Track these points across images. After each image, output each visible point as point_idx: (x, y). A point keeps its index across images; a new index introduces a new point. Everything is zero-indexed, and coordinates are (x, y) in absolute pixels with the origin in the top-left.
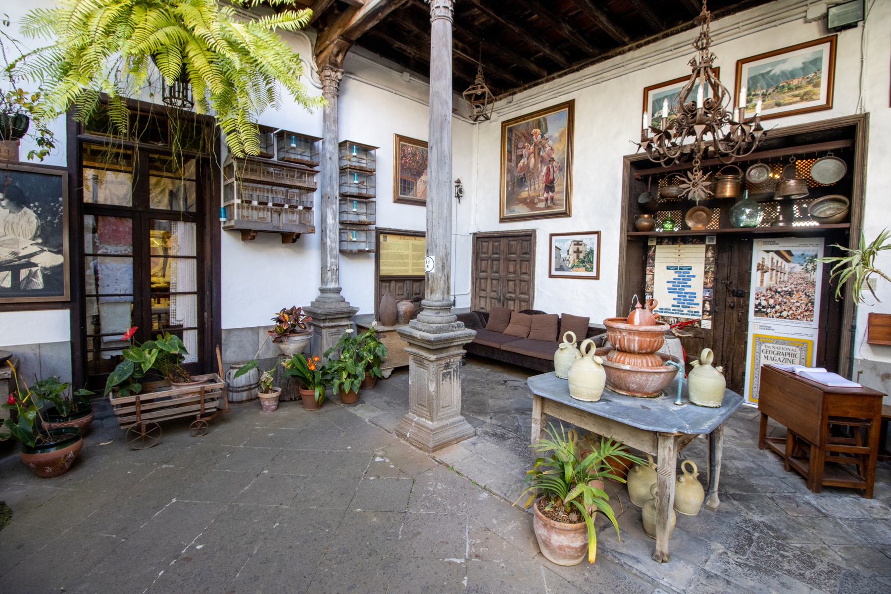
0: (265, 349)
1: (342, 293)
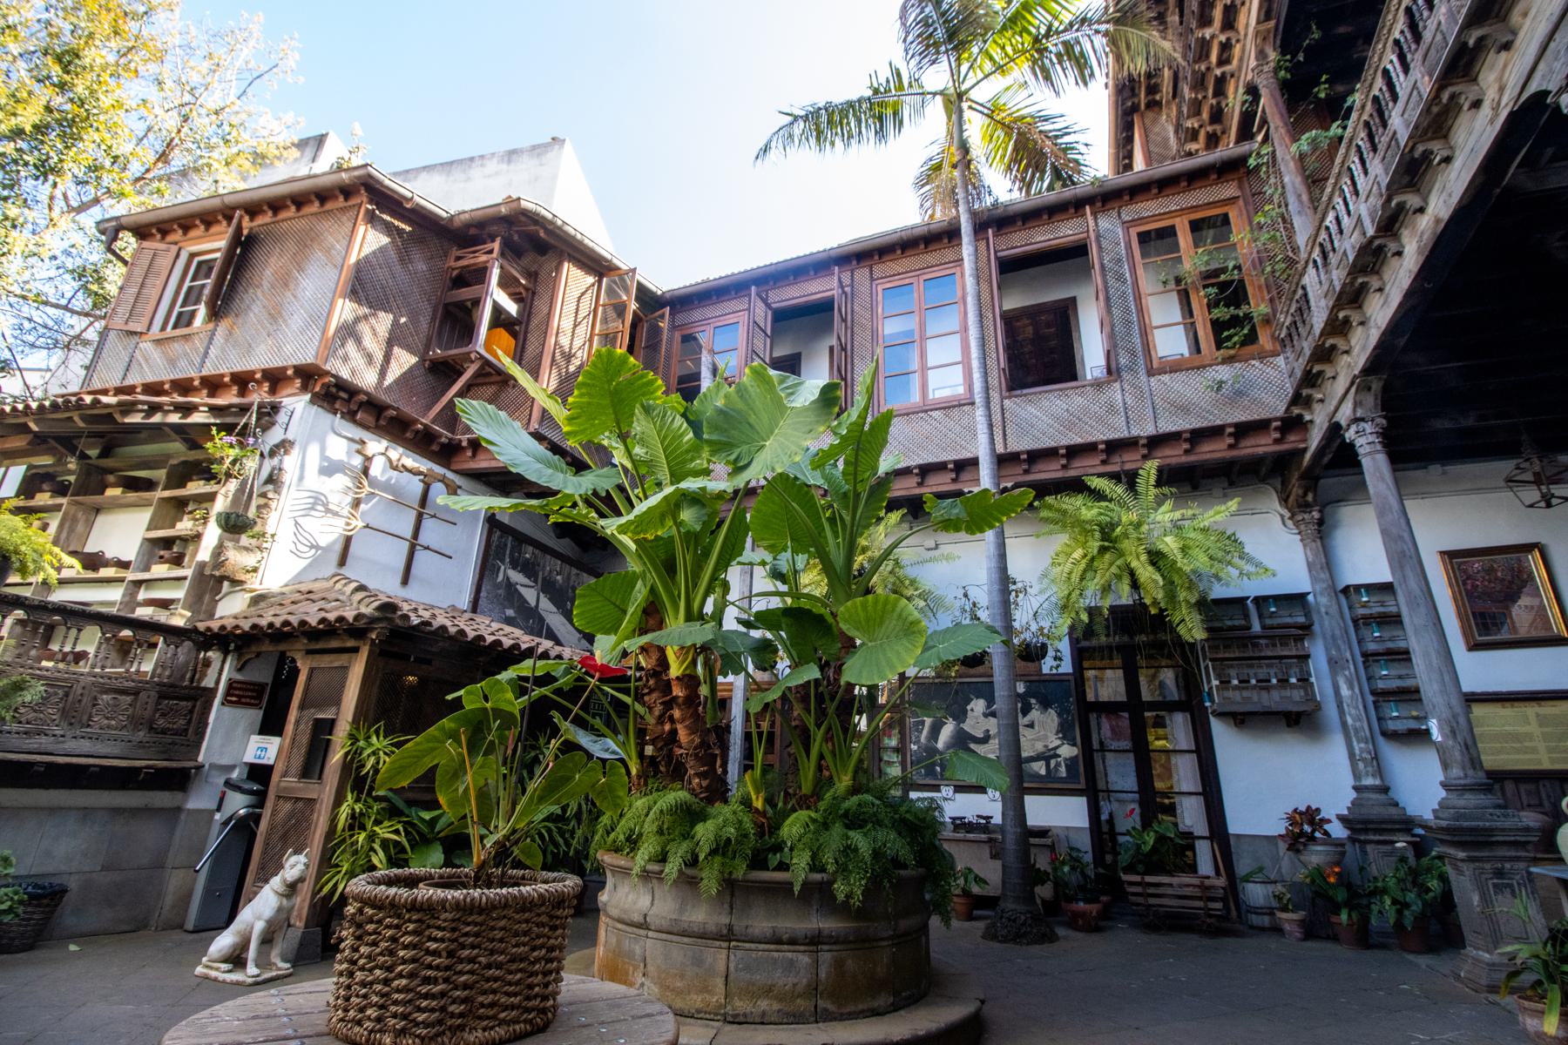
0: (1287, 865)
1: (1391, 794)
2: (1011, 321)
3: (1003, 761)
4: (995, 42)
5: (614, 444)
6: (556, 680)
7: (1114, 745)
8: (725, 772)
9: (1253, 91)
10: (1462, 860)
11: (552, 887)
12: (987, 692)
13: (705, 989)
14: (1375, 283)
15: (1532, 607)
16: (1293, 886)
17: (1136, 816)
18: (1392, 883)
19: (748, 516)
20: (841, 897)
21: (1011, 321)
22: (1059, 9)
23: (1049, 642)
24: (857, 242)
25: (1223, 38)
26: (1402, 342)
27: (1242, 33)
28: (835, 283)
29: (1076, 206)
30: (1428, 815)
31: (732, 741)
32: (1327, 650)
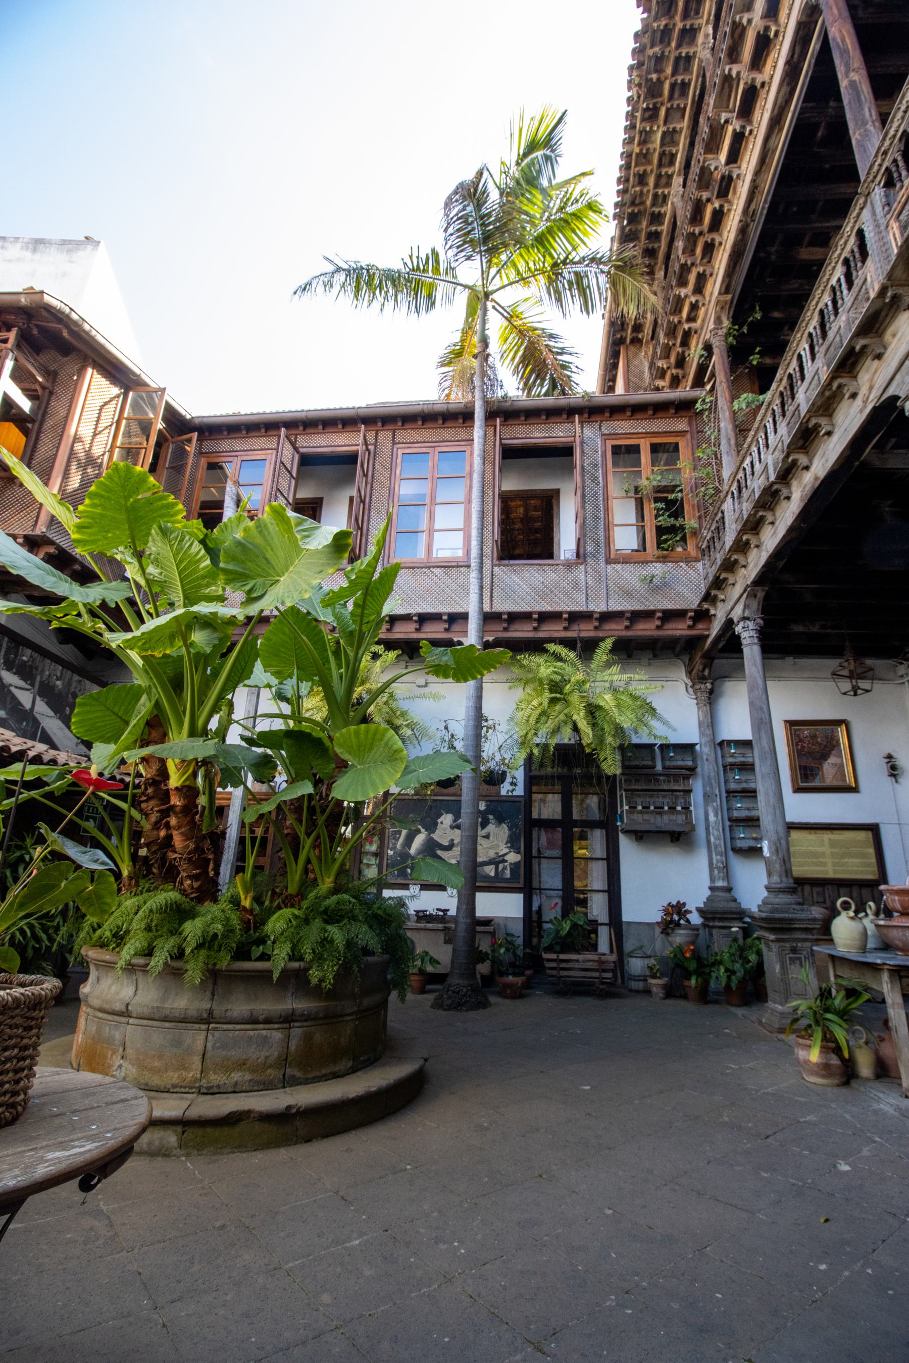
0: (662, 947)
1: (733, 893)
2: (506, 499)
3: (462, 865)
4: (521, 255)
5: (129, 559)
6: (47, 784)
7: (548, 853)
8: (217, 874)
9: (708, 348)
10: (772, 941)
11: (28, 991)
12: (455, 808)
13: (183, 1067)
14: (770, 518)
15: (836, 765)
16: (662, 960)
17: (559, 908)
18: (726, 956)
19: (259, 642)
20: (314, 981)
21: (506, 499)
22: (578, 241)
23: (508, 771)
24: (384, 405)
25: (693, 299)
26: (781, 564)
27: (707, 299)
28: (361, 440)
29: (568, 413)
30: (754, 909)
31: (226, 846)
32: (704, 786)
